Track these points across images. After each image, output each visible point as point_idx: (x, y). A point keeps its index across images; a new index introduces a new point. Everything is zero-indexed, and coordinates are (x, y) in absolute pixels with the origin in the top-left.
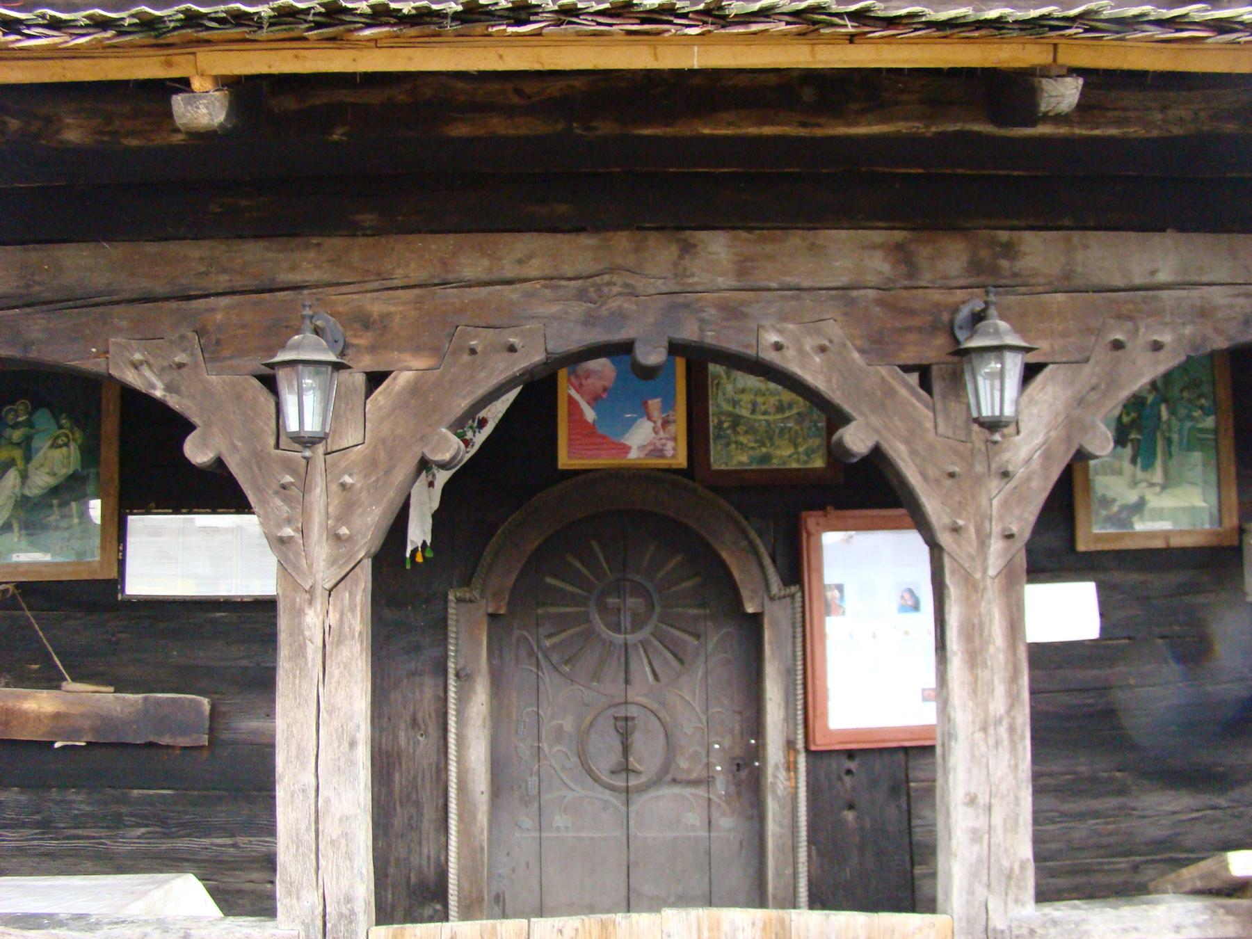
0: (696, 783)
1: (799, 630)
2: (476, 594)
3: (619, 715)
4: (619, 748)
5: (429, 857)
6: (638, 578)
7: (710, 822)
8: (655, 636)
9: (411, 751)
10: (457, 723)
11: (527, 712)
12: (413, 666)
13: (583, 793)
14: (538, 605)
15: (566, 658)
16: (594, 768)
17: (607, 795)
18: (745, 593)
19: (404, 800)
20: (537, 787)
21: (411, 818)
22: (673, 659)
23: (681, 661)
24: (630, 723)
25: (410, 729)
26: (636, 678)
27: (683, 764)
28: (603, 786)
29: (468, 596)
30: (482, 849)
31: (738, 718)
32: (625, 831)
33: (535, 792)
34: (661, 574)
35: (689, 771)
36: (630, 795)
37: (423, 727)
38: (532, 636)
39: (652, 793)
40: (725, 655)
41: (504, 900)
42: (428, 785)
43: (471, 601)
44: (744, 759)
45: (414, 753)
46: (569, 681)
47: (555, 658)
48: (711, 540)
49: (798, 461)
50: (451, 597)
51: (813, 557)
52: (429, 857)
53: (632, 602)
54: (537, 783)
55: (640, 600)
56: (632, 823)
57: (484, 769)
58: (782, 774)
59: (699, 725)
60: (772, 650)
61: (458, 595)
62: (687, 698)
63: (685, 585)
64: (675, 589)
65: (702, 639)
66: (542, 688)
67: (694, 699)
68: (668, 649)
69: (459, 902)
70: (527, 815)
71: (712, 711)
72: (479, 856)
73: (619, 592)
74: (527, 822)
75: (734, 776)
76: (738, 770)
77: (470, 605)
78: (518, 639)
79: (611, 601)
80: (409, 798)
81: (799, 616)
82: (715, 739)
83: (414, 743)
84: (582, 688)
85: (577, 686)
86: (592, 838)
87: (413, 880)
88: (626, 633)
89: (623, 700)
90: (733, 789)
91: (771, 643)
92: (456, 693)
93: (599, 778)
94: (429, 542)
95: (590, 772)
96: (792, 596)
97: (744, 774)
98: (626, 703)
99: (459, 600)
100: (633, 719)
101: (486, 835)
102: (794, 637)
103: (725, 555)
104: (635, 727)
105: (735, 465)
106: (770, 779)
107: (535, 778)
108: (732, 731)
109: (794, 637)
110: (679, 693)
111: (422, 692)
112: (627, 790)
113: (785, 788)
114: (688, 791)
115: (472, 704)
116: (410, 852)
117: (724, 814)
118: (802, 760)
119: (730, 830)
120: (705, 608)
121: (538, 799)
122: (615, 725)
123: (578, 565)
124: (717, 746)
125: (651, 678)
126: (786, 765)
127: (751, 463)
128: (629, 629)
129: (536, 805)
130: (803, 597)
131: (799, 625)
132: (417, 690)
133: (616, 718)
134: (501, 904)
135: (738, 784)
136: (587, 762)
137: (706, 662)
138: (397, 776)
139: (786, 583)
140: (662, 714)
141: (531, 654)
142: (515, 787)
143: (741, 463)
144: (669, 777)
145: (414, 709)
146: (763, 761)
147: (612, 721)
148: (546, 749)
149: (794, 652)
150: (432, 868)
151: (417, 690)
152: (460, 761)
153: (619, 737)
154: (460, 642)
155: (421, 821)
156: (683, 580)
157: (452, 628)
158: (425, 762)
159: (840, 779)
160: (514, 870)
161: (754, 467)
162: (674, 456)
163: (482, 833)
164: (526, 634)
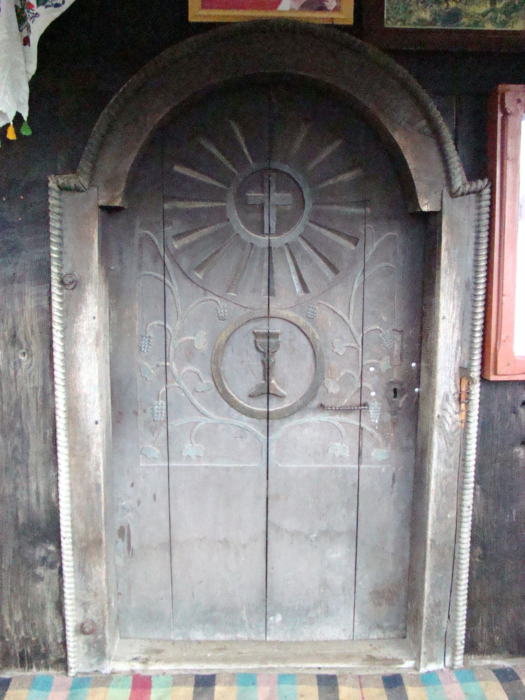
0: (347, 410)
1: (484, 235)
2: (83, 181)
3: (261, 331)
4: (260, 369)
5: (38, 494)
6: (286, 169)
7: (360, 454)
8: (304, 239)
9: (12, 372)
10: (63, 339)
11: (153, 327)
12: (10, 270)
13: (215, 418)
14: (165, 199)
16: (230, 391)
17: (245, 421)
18: (420, 187)
20: (164, 412)
21: (15, 449)
22: (325, 266)
23: (335, 270)
24: (272, 341)
25: (9, 347)
26: (280, 288)
27: (333, 387)
28: (239, 411)
29: (73, 183)
30: (98, 486)
31: (398, 337)
33: (163, 417)
34: (311, 166)
35: (339, 396)
37: (25, 345)
38: (158, 240)
39: (296, 420)
40: (387, 264)
41: (129, 531)
42: (33, 412)
43: (77, 190)
44: (401, 384)
45: (15, 375)
46: (201, 291)
47: (185, 263)
48: (384, 121)
49: (493, 20)
50: (51, 184)
51: (510, 142)
52: (38, 494)
53: (276, 197)
54: (165, 407)
55: (289, 195)
56: (272, 452)
57: (97, 395)
58: (452, 407)
60: (449, 259)
61: (61, 181)
62: (340, 312)
63: (341, 178)
65: (360, 244)
66: (169, 297)
68: (319, 254)
69: (73, 543)
70: (154, 443)
72: (94, 495)
73: (262, 186)
74: (156, 452)
75: (390, 403)
76: (395, 396)
77: (78, 195)
78: (141, 240)
79: (255, 196)
80: (12, 427)
81: (485, 217)
82: (369, 361)
83: (15, 364)
84: (216, 299)
85: (210, 297)
86: (227, 469)
87: (22, 519)
88: (269, 234)
90: (388, 417)
91: (448, 249)
92: (61, 304)
93: (236, 402)
94: (25, 115)
95: (225, 395)
96: (478, 193)
97: (401, 401)
98: (269, 317)
99: (62, 189)
100: (276, 335)
101: (102, 471)
102: (477, 243)
103: (398, 137)
104: (278, 345)
105: (414, 23)
106: (438, 412)
108: (390, 354)
109: (477, 243)
110: (331, 307)
111: (22, 302)
112: (268, 416)
113: (454, 423)
114: (336, 419)
116: (16, 488)
117: (377, 445)
118: (476, 390)
119: (383, 462)
121: (165, 424)
122: (255, 342)
123: (214, 151)
124: (372, 369)
125: (298, 289)
126: (457, 396)
127: (434, 21)
128: (273, 230)
129: (163, 433)
130: (493, 193)
131: (484, 229)
132: (16, 300)
133: (256, 335)
134: (126, 539)
135: (394, 413)
136: (222, 385)
139: (472, 176)
140: (311, 330)
141: (157, 257)
142: (140, 412)
143: (421, 21)
144: (316, 403)
145: (14, 322)
146: (431, 388)
147: (252, 338)
148: (175, 370)
149: (476, 262)
150: (42, 507)
151: (16, 300)
152: (69, 385)
153: (260, 356)
154: (65, 240)
155: (28, 454)
156: (344, 171)
157: (54, 224)
158: (29, 386)
159: (515, 412)
160: (139, 503)
161: (439, 26)
162: (337, 9)
163: (97, 469)
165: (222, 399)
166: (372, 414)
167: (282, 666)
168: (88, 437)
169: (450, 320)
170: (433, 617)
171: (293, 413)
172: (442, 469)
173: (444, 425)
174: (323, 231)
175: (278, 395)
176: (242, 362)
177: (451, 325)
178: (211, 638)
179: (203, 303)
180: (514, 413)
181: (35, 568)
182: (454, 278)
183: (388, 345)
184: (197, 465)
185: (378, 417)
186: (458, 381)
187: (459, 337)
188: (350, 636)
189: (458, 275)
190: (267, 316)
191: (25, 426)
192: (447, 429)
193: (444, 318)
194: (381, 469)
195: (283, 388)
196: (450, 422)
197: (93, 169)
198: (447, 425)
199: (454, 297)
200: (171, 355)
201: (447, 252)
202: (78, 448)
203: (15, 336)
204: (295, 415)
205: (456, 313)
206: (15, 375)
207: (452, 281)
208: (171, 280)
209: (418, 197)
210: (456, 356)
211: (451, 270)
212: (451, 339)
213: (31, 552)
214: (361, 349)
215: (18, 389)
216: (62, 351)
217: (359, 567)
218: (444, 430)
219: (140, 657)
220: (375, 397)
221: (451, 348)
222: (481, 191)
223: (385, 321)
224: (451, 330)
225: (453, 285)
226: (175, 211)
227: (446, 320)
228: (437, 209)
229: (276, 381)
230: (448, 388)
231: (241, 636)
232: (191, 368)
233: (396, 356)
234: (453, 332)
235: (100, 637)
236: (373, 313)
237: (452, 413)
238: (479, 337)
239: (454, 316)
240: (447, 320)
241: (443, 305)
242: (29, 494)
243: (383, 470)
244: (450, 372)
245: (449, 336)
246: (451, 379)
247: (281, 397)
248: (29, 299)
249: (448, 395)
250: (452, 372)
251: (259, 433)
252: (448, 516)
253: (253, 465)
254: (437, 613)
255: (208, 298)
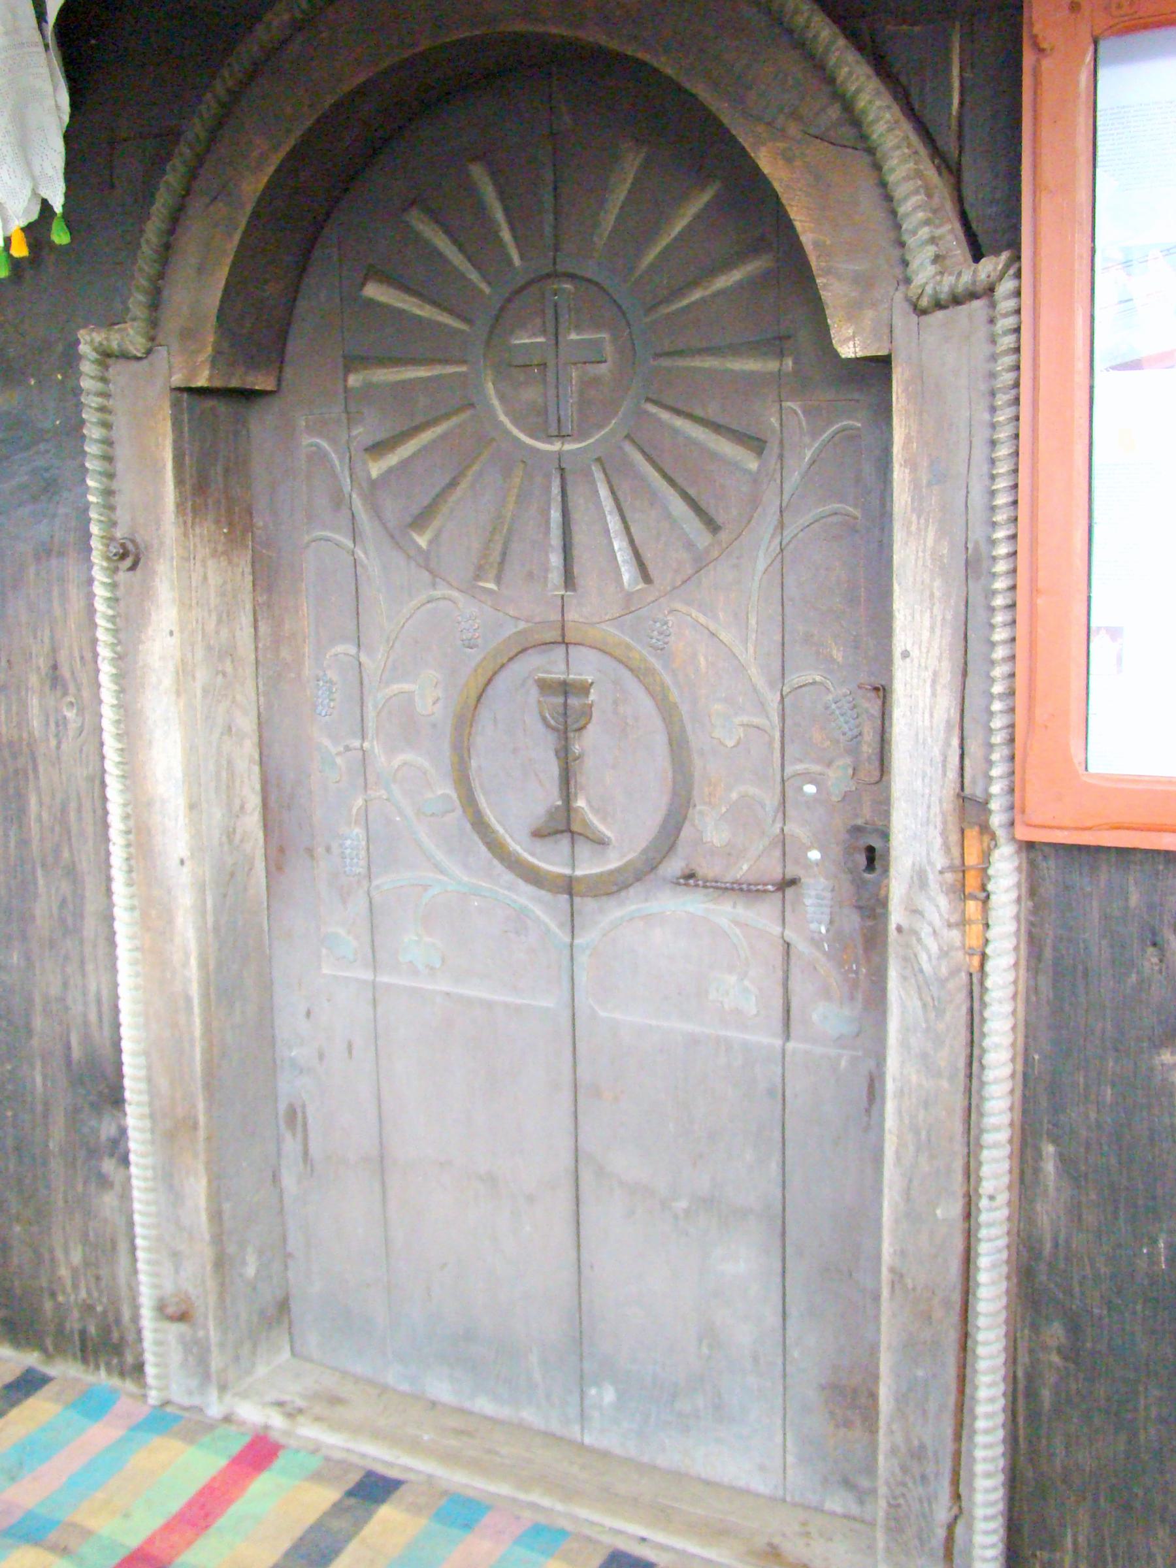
0: (746, 890)
14: (351, 363)
15: (415, 510)
17: (525, 895)
19: (50, 860)
21: (64, 902)
23: (712, 526)
24: (573, 702)
30: (188, 1000)
32: (566, 995)
33: (361, 870)
35: (731, 853)
36: (577, 900)
39: (632, 904)
45: (58, 747)
47: (392, 508)
50: (83, 348)
59: (756, 720)
64: (696, 295)
67: (745, 641)
68: (672, 482)
71: (794, 679)
82: (799, 767)
83: (57, 725)
86: (489, 1005)
89: (554, 635)
91: (911, 464)
95: (480, 825)
103: (766, 161)
104: (587, 713)
107: (358, 831)
113: (944, 953)
115: (150, 632)
116: (65, 984)
117: (825, 993)
119: (840, 1041)
120: (781, 355)
123: (442, 243)
124: (810, 789)
125: (628, 573)
129: (363, 903)
134: (299, 1135)
137: (781, 526)
138: (33, 800)
142: (320, 850)
144: (674, 866)
145: (52, 638)
155: (82, 916)
156: (728, 265)
160: (321, 1056)
163: (185, 964)
164: (324, 444)
165: (476, 838)
166: (810, 909)
167: (559, 1507)
168: (169, 891)
169: (923, 661)
170: (903, 1484)
171: (626, 886)
172: (914, 1078)
173: (916, 956)
174: (679, 423)
175: (590, 835)
176: (515, 751)
177: (928, 675)
178: (467, 1404)
179: (429, 606)
180: (1154, 944)
181: (100, 1159)
182: (930, 542)
183: (846, 728)
184: (430, 987)
185: (827, 918)
186: (954, 837)
187: (952, 711)
188: (776, 1487)
189: (942, 533)
190: (560, 639)
191: (76, 859)
192: (926, 966)
193: (905, 655)
194: (840, 1056)
195: (604, 819)
196: (934, 947)
197: (155, 304)
198: (923, 957)
199: (932, 595)
200: (371, 724)
201: (907, 471)
202: (154, 913)
203: (55, 667)
204: (631, 890)
205: (941, 642)
206: (58, 747)
207: (924, 551)
208: (366, 553)
209: (829, 321)
210: (944, 766)
211: (922, 521)
212: (927, 716)
213: (94, 1123)
214: (777, 735)
215: (64, 777)
216: (115, 702)
217: (793, 1312)
218: (916, 968)
219: (293, 1402)
220: (817, 865)
221: (929, 740)
222: (991, 290)
223: (840, 659)
224: (929, 690)
225: (929, 563)
226: (368, 392)
227: (912, 661)
228: (878, 349)
229: (589, 802)
230: (924, 853)
231: (529, 1415)
232: (409, 756)
233: (869, 758)
234: (934, 694)
235: (201, 1334)
236: (807, 639)
237: (938, 923)
238: (1001, 712)
239: (935, 651)
240: (916, 662)
241: (903, 618)
242: (85, 1004)
243: (843, 1063)
244: (929, 807)
245: (921, 705)
246: (931, 828)
247: (601, 842)
248: (75, 590)
249: (926, 871)
250: (935, 809)
251: (553, 926)
252: (939, 1212)
253: (544, 1004)
254: (918, 1478)
255: (437, 593)
